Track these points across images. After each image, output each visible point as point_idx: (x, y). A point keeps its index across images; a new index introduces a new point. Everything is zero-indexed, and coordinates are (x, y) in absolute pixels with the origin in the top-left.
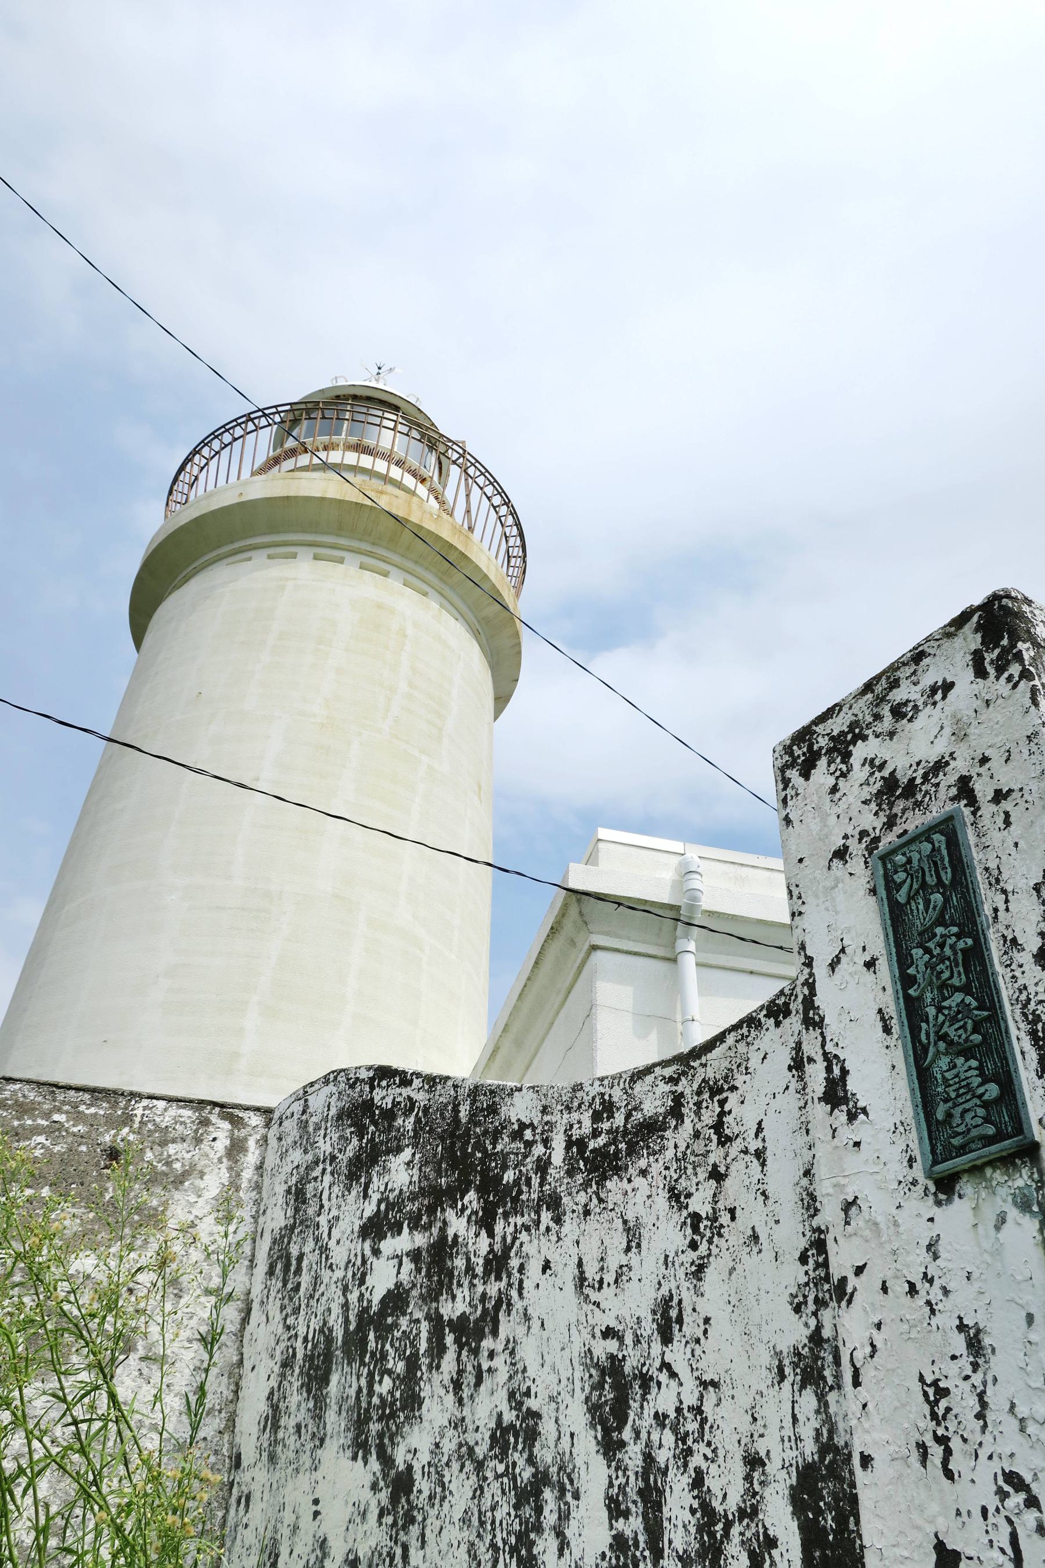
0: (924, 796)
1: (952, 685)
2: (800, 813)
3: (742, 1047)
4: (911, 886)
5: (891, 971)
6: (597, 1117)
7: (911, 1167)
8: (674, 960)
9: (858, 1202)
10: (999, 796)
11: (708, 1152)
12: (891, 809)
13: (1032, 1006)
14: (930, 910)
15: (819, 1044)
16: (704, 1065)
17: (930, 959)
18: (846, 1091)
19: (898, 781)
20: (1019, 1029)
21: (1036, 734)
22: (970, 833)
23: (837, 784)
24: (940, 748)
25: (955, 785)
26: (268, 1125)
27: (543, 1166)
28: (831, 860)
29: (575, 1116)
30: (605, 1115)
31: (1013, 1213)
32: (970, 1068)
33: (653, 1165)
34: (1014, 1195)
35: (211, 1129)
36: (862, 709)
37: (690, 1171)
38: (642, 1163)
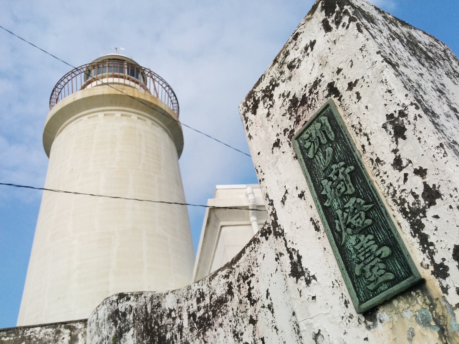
0: (312, 101)
1: (315, 41)
2: (255, 131)
3: (253, 254)
4: (314, 148)
5: (313, 196)
6: (198, 301)
7: (347, 307)
8: (251, 225)
9: (321, 333)
10: (351, 86)
11: (247, 310)
12: (296, 114)
13: (398, 195)
14: (327, 157)
15: (284, 244)
16: (238, 266)
17: (332, 184)
18: (302, 268)
19: (297, 98)
20: (393, 210)
21: (364, 46)
22: (340, 110)
23: (269, 112)
24: (315, 75)
25: (326, 89)
26: (86, 327)
27: (180, 329)
28: (273, 148)
29: (190, 302)
30: (201, 299)
31: (418, 328)
32: (369, 240)
33: (224, 320)
34: (415, 316)
35: (61, 334)
36: (274, 72)
37: (240, 321)
38: (220, 320)
